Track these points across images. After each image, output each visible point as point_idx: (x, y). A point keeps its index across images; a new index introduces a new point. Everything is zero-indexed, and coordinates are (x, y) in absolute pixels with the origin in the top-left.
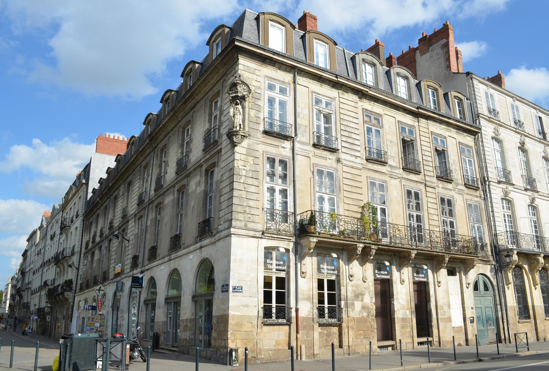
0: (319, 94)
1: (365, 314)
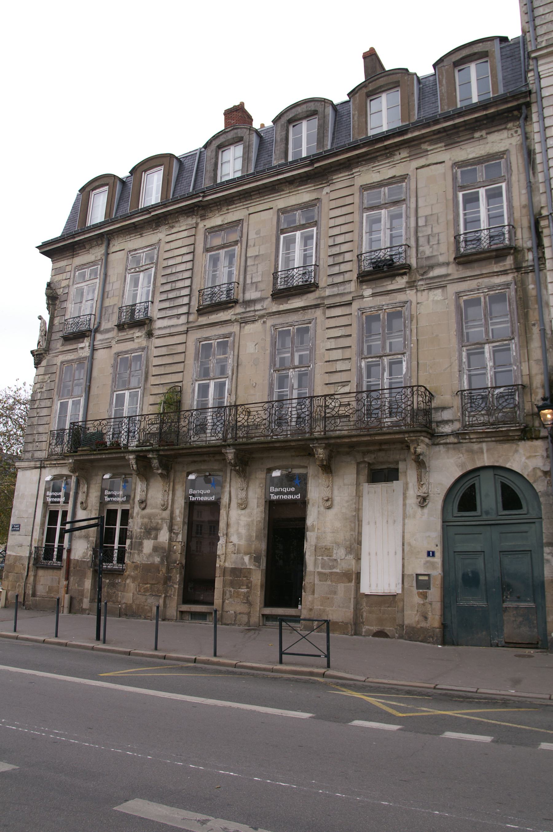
0: (136, 250)
1: (157, 560)
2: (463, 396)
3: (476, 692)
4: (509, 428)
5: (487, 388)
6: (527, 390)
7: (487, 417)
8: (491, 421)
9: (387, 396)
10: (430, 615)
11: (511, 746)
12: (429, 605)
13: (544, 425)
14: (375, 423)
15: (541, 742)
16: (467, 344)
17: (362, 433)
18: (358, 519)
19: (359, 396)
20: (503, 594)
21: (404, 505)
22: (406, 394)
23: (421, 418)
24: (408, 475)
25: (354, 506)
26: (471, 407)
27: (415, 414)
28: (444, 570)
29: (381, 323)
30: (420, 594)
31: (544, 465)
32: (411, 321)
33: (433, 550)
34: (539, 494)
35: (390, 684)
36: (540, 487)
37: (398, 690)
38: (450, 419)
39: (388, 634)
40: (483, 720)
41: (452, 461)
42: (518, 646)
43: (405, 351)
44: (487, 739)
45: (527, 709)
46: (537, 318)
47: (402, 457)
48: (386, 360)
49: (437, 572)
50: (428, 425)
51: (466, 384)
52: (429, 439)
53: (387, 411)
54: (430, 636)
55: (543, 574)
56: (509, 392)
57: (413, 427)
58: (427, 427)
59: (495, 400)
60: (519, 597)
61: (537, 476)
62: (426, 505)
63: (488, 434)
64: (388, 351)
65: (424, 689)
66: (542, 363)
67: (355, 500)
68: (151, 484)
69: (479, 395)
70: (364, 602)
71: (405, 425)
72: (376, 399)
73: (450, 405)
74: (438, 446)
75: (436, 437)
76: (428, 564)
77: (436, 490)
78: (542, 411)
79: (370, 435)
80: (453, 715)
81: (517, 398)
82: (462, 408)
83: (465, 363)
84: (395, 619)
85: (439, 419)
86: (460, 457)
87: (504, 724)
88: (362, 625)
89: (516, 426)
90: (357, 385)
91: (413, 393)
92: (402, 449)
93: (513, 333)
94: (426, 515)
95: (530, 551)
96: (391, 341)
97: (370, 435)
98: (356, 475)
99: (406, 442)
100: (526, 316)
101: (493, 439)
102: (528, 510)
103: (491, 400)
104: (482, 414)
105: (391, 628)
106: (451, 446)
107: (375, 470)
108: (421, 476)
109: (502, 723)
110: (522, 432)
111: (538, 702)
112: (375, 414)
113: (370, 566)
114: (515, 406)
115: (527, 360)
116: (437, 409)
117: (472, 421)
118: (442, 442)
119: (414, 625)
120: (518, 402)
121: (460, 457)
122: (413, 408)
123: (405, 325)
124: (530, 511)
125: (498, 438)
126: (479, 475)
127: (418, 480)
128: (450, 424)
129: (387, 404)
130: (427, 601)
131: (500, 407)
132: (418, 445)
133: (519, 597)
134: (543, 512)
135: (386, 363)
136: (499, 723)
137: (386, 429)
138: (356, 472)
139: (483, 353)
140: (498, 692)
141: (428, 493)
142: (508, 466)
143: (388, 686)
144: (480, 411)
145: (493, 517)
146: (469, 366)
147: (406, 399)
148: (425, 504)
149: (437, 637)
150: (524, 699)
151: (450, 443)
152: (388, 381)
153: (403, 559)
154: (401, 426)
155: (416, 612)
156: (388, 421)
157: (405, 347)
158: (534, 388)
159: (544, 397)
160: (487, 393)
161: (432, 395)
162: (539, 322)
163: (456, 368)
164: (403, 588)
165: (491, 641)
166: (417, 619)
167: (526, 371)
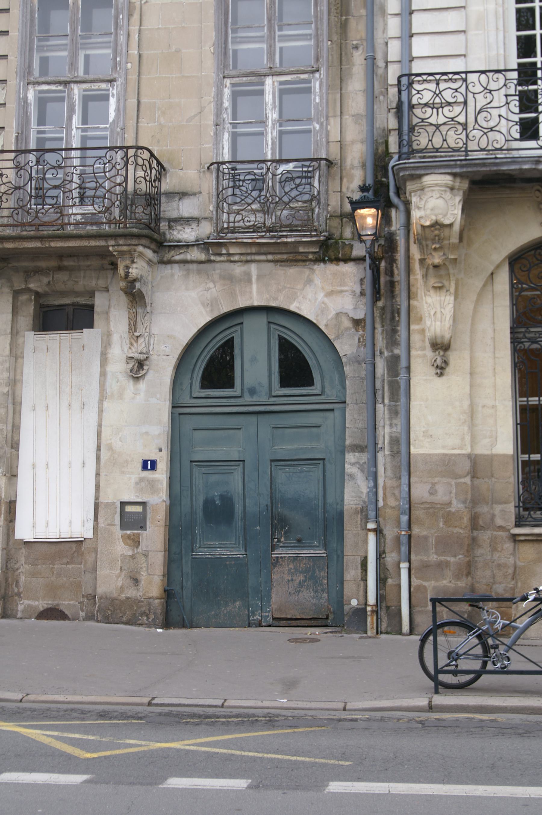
2: (221, 174)
3: (222, 706)
4: (298, 239)
5: (264, 161)
6: (335, 170)
7: (261, 215)
8: (269, 223)
9: (76, 162)
10: (143, 576)
11: (280, 792)
12: (143, 558)
13: (360, 236)
14: (52, 216)
15: (329, 780)
16: (234, 73)
17: (25, 233)
18: (14, 399)
19: (22, 158)
20: (273, 534)
21: (103, 374)
22: (113, 162)
23: (140, 210)
24: (112, 318)
25: (6, 375)
26: (234, 195)
27: (129, 202)
28: (171, 495)
29: (70, 15)
30: (126, 539)
31: (355, 308)
32: (130, 15)
33: (153, 458)
34: (344, 360)
35: (69, 703)
36: (346, 347)
37: (83, 712)
38: (193, 214)
39: (67, 612)
40: (233, 752)
41: (194, 294)
42: (294, 623)
43: (115, 76)
44: (241, 784)
45: (307, 729)
46: (363, 34)
47: (102, 283)
48: (76, 91)
49: (159, 499)
50: (153, 225)
51: (226, 150)
52: (154, 252)
53: (75, 194)
54: (143, 614)
55: (343, 500)
56: (302, 171)
57: (125, 227)
58: (150, 228)
59: (278, 184)
60: (299, 541)
61: (342, 328)
62: (144, 375)
63: (262, 248)
64: (81, 72)
65: (130, 707)
66: (364, 122)
67: (7, 365)
68: (133, 190)
69: (249, 173)
70: (22, 555)
71: (109, 222)
72: (54, 167)
73: (196, 189)
74: (169, 266)
75: (167, 249)
76: (143, 484)
77: (163, 347)
78: (358, 210)
79: (41, 238)
80: (183, 747)
81: (316, 184)
82: (218, 195)
83: (226, 109)
84: (79, 585)
85: (174, 214)
86: (209, 289)
87: (269, 756)
88: (16, 598)
89: (312, 236)
90: (17, 137)
91: (128, 160)
92: (102, 268)
93: (317, 60)
94: (142, 394)
95: (323, 459)
96: (89, 52)
97: (41, 238)
98: (10, 316)
99: (111, 254)
100: (344, 27)
101: (270, 257)
102: (323, 388)
103: (270, 184)
104: (252, 210)
105: (72, 602)
106: (194, 266)
107: (48, 306)
108: (136, 321)
109: (266, 755)
110: (321, 247)
111: (326, 715)
112: (52, 197)
113: (34, 489)
114: (313, 198)
115: (339, 113)
116: (170, 195)
117: (234, 222)
118: (177, 258)
119: (115, 595)
120: (319, 192)
121: (209, 289)
122: (126, 189)
123: (116, 23)
124: (326, 390)
125: (279, 257)
126: (242, 323)
127: (130, 329)
128: (194, 225)
129: (76, 178)
130: (139, 550)
131: (286, 199)
132: (133, 262)
133: (299, 541)
134: (348, 392)
135: (76, 97)
136: (260, 755)
137: (72, 227)
138: (10, 310)
139: (261, 93)
140: (259, 704)
141: (148, 353)
142: (293, 308)
143: (65, 706)
144: (249, 205)
145: (264, 399)
146: (235, 116)
147: (113, 172)
148: (142, 373)
149: (154, 613)
150: (303, 712)
151: (192, 262)
152: (80, 132)
153: (98, 474)
154: (102, 223)
155: (119, 571)
156: (76, 212)
157: (115, 67)
158: (348, 167)
159: (364, 185)
160: (264, 171)
161: (162, 167)
162: (365, 44)
163: (210, 119)
164: (96, 528)
165: (249, 617)
166: (120, 584)
167: (335, 136)
